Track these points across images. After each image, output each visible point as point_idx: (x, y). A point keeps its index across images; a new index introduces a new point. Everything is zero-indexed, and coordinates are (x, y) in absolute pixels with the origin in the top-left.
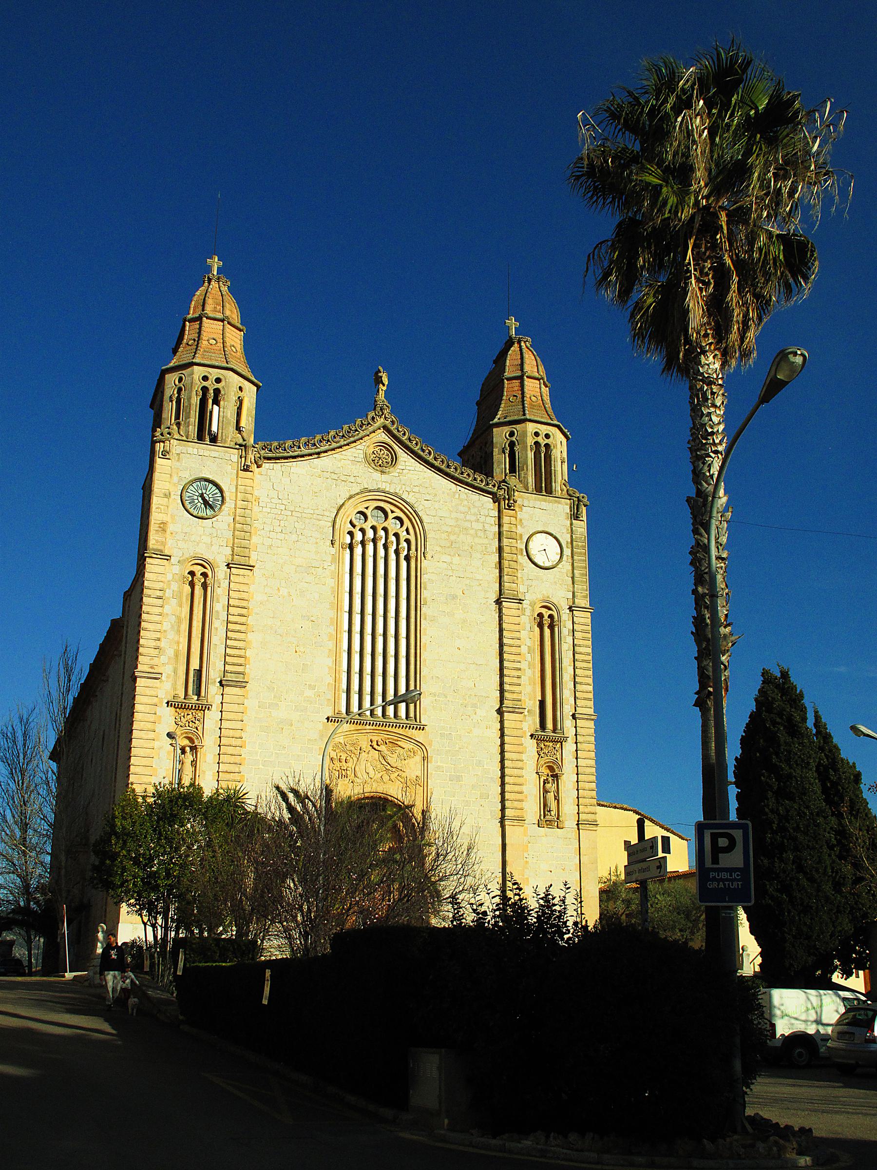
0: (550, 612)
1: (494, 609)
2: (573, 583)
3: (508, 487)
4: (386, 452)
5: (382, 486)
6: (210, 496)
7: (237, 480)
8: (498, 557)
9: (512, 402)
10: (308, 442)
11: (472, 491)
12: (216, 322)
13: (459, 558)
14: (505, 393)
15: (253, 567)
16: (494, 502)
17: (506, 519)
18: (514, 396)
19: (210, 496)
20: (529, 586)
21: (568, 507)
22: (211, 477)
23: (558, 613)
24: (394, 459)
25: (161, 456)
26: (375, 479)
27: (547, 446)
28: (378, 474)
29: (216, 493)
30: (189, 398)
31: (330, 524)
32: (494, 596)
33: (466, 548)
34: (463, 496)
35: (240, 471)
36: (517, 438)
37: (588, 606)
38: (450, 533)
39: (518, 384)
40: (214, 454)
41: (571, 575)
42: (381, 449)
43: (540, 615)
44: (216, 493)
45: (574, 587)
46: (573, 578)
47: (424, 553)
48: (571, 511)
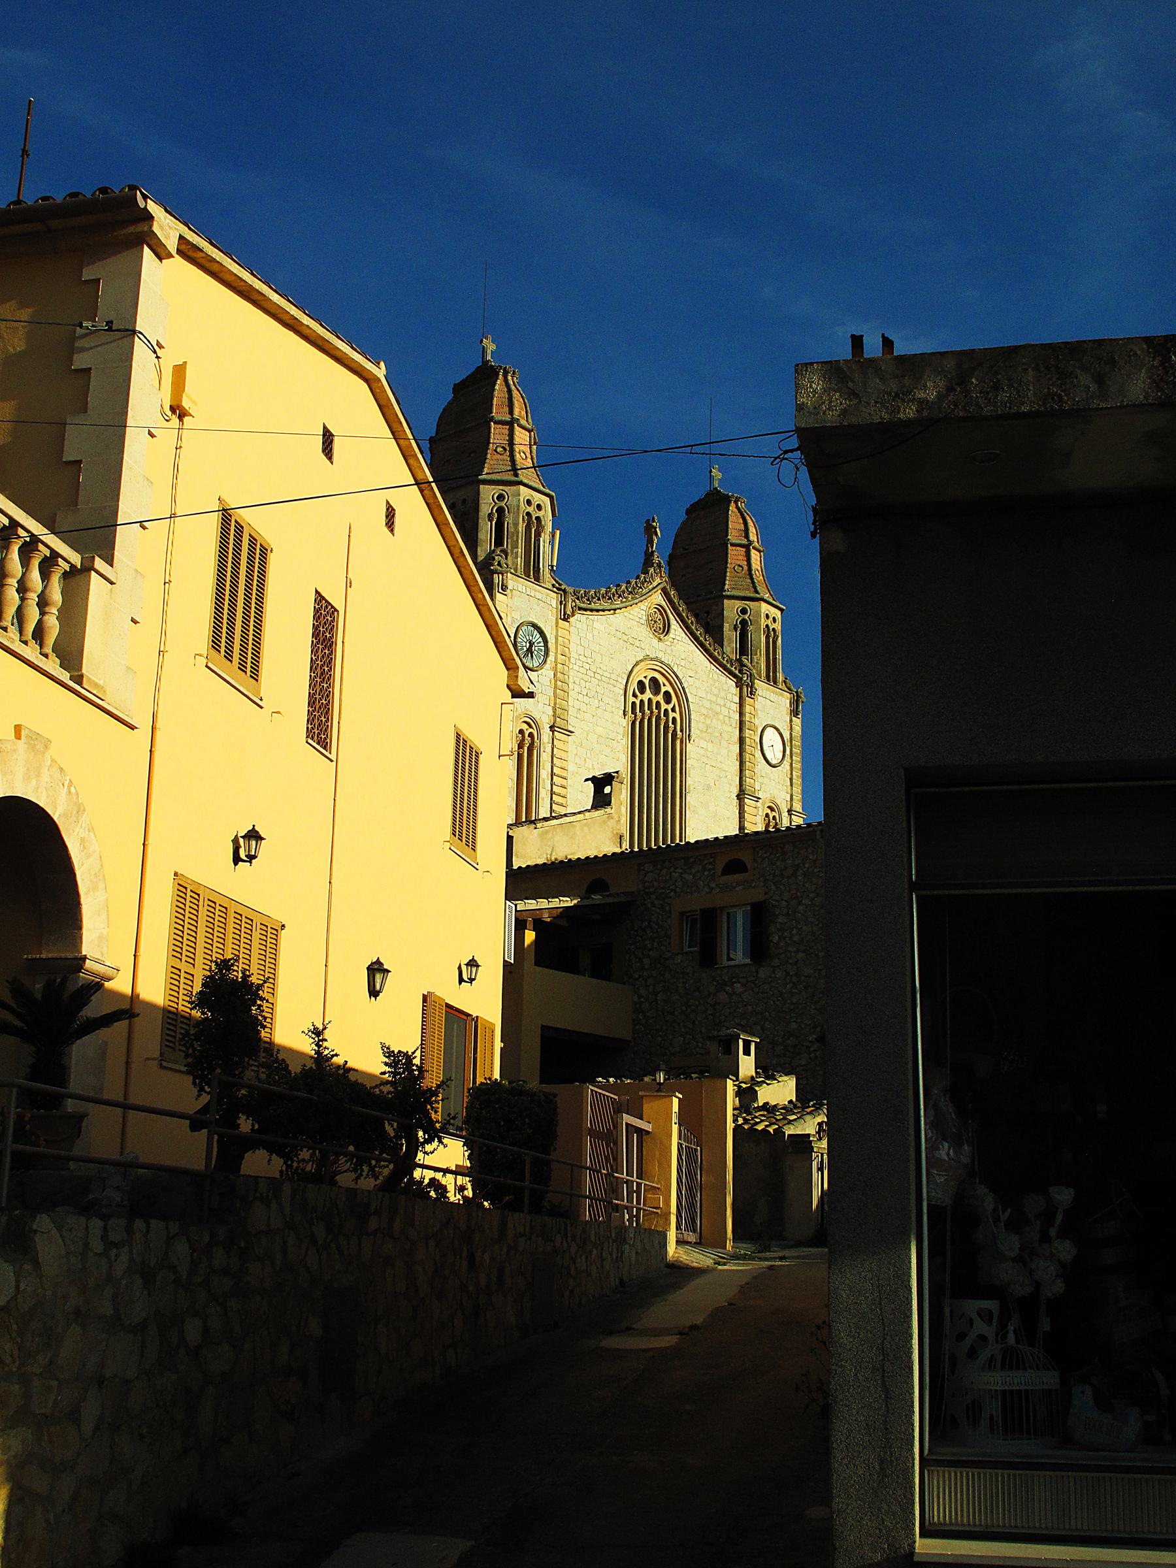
0: (531, 730)
1: (735, 805)
2: (791, 785)
3: (750, 673)
4: (659, 616)
5: (660, 655)
6: (536, 648)
7: (557, 630)
8: (738, 748)
9: (738, 573)
10: (606, 594)
11: (722, 672)
12: (524, 431)
13: (712, 744)
14: (729, 560)
15: (760, 799)
16: (737, 687)
17: (748, 709)
18: (739, 566)
19: (536, 648)
20: (762, 784)
21: (788, 701)
22: (540, 624)
23: (780, 815)
24: (666, 629)
25: (500, 590)
26: (652, 645)
27: (538, 518)
28: (655, 641)
29: (540, 642)
30: (516, 525)
31: (622, 692)
32: (736, 791)
33: (717, 734)
34: (715, 677)
35: (560, 620)
36: (750, 617)
37: (801, 811)
38: (706, 716)
39: (743, 553)
40: (538, 595)
41: (789, 776)
42: (655, 612)
43: (521, 732)
44: (540, 642)
45: (792, 789)
46: (791, 779)
47: (689, 735)
48: (791, 706)
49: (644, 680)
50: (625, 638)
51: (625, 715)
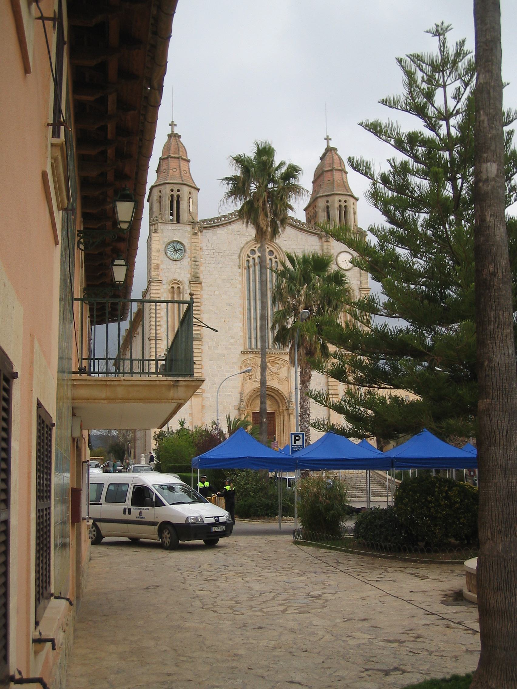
30: (165, 201)
49: (255, 249)
50: (239, 233)
51: (239, 267)
